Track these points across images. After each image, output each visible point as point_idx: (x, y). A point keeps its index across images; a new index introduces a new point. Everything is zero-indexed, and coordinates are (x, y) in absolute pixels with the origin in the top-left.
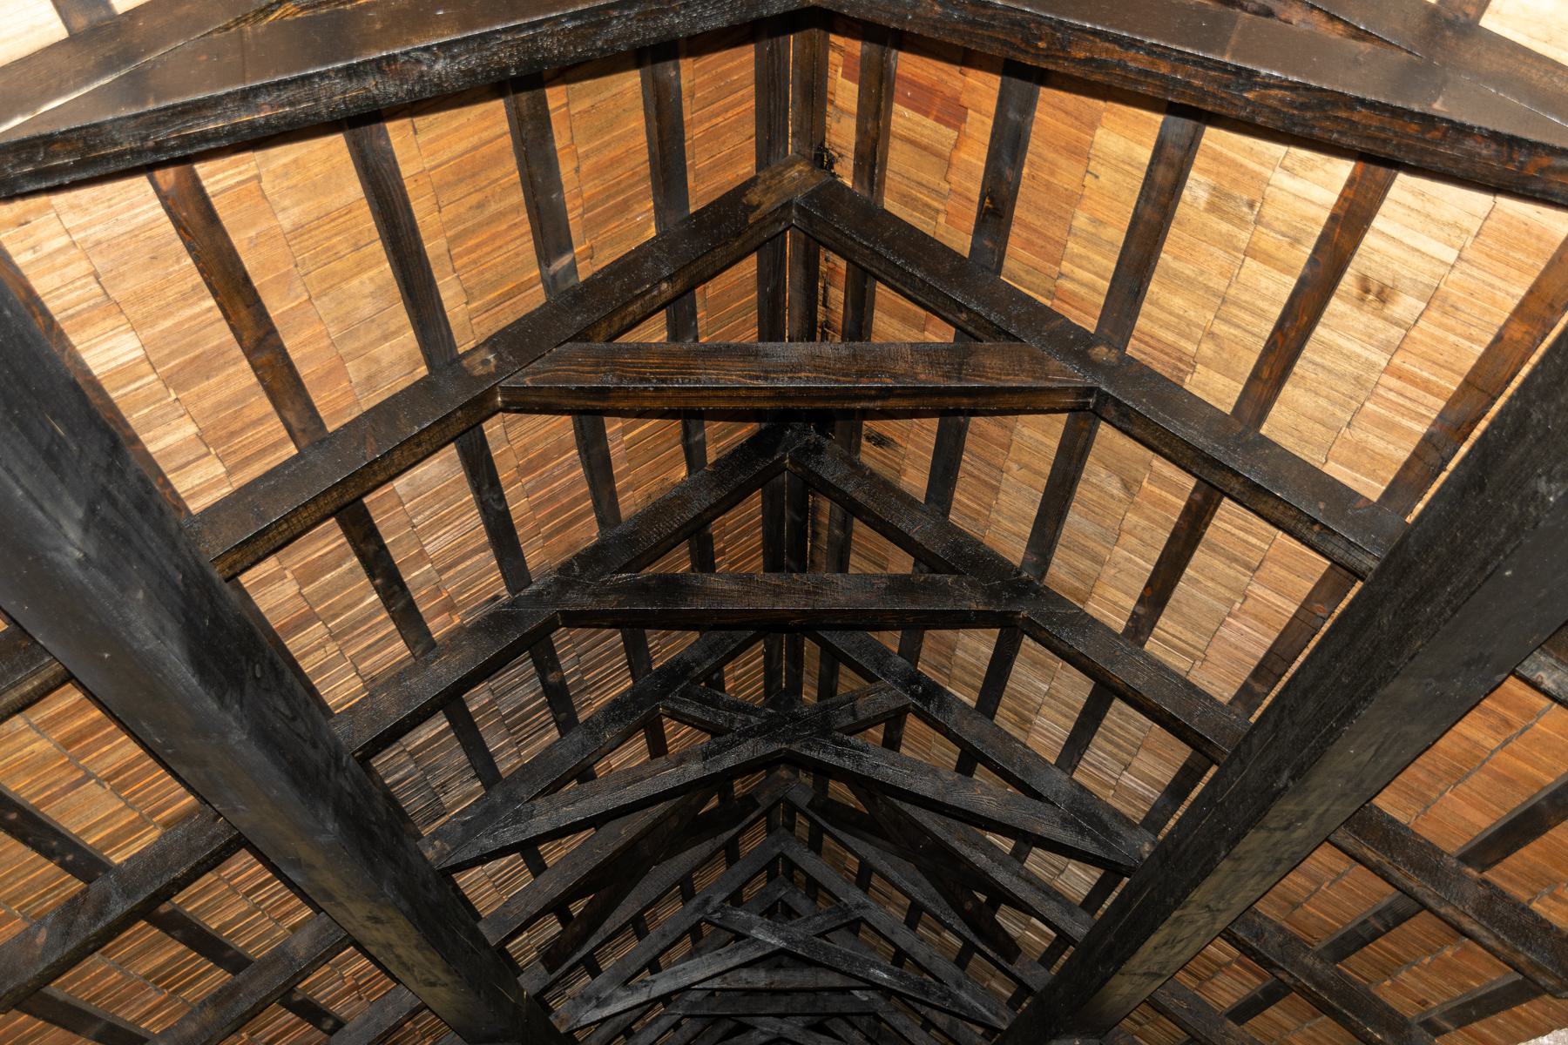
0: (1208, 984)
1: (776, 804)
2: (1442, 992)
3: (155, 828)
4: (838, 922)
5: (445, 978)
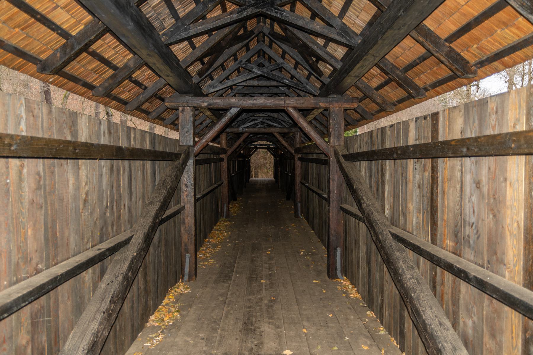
0: (371, 81)
1: (260, 33)
2: (431, 80)
3: (82, 25)
4: (276, 68)
5: (171, 74)
